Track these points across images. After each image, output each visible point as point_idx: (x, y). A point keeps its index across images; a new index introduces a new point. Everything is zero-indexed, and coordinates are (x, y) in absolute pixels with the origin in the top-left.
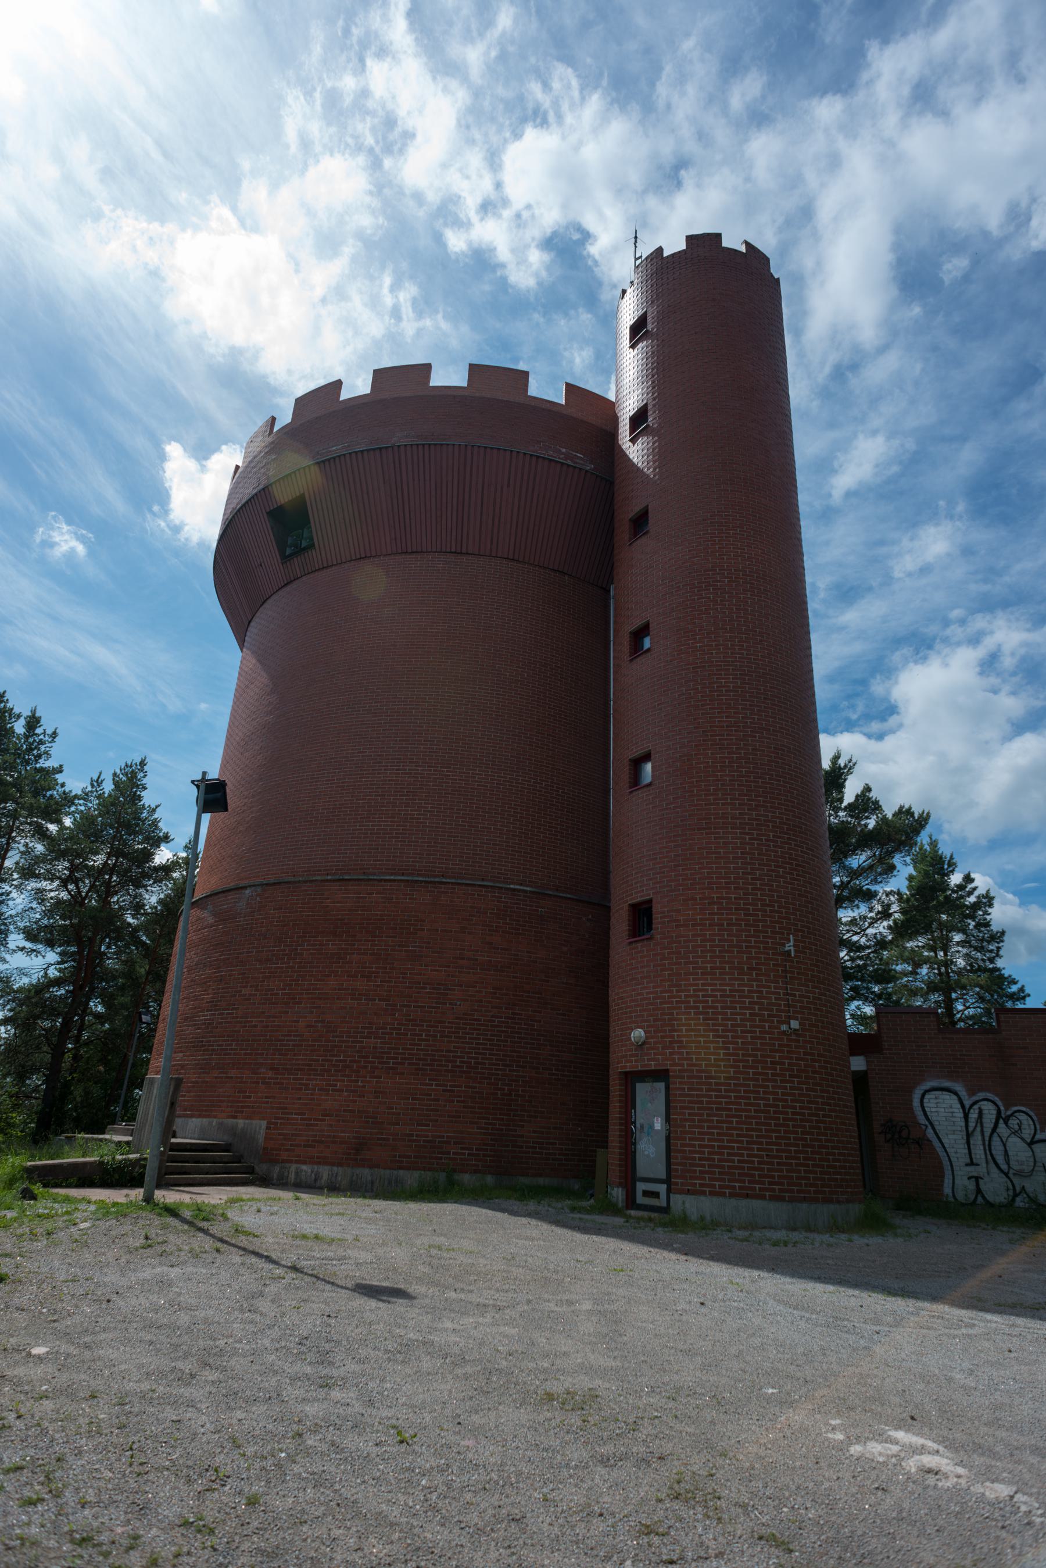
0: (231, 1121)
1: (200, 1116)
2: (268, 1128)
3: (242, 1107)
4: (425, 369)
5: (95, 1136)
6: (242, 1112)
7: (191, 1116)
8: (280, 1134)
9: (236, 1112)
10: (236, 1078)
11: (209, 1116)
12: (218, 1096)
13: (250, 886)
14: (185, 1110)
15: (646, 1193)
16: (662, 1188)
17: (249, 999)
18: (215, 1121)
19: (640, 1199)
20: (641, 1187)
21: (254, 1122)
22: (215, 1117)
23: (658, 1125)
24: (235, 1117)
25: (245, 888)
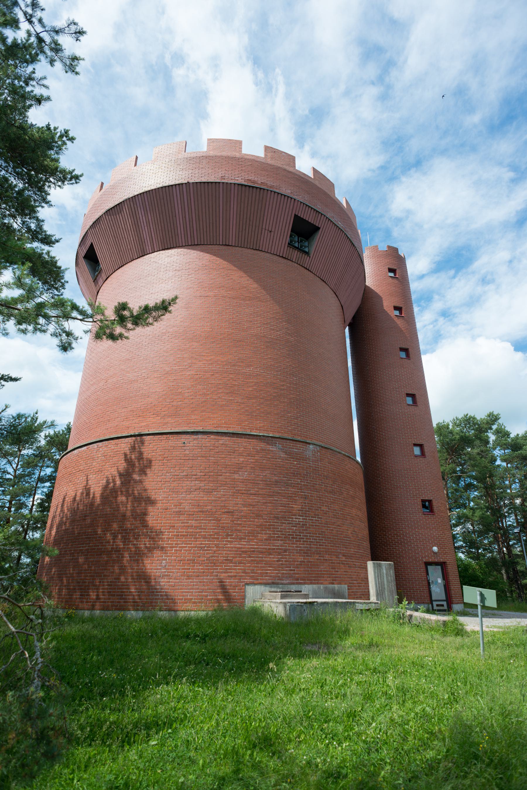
0: (331, 586)
1: (311, 583)
2: (348, 589)
3: (335, 577)
4: (239, 143)
5: (359, 601)
6: (336, 580)
7: (304, 584)
8: (352, 592)
9: (333, 580)
10: (329, 560)
11: (318, 583)
12: (321, 571)
13: (313, 444)
14: (298, 580)
15: (437, 605)
16: (445, 603)
17: (326, 514)
18: (322, 586)
19: (435, 607)
20: (435, 603)
21: (342, 586)
22: (322, 584)
23: (440, 581)
24: (333, 584)
25: (309, 444)
